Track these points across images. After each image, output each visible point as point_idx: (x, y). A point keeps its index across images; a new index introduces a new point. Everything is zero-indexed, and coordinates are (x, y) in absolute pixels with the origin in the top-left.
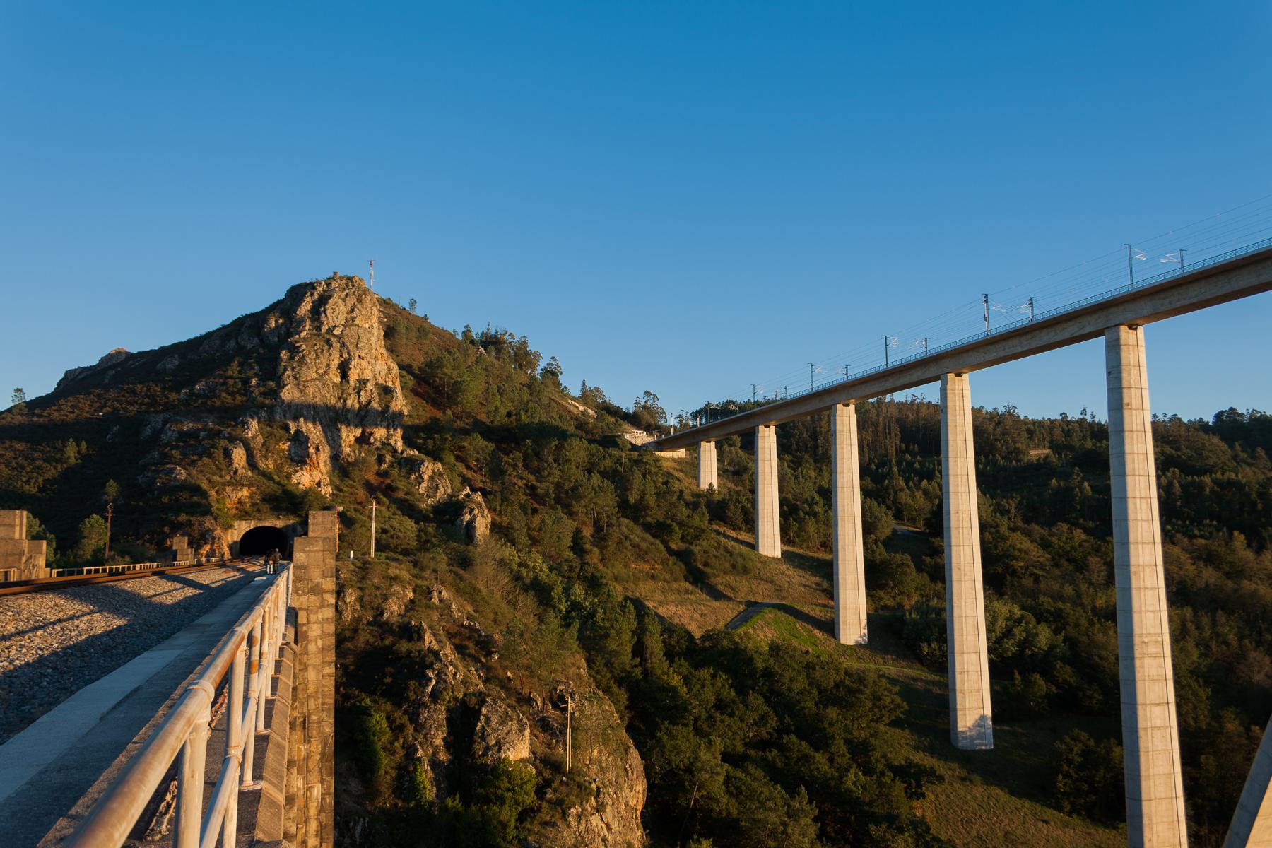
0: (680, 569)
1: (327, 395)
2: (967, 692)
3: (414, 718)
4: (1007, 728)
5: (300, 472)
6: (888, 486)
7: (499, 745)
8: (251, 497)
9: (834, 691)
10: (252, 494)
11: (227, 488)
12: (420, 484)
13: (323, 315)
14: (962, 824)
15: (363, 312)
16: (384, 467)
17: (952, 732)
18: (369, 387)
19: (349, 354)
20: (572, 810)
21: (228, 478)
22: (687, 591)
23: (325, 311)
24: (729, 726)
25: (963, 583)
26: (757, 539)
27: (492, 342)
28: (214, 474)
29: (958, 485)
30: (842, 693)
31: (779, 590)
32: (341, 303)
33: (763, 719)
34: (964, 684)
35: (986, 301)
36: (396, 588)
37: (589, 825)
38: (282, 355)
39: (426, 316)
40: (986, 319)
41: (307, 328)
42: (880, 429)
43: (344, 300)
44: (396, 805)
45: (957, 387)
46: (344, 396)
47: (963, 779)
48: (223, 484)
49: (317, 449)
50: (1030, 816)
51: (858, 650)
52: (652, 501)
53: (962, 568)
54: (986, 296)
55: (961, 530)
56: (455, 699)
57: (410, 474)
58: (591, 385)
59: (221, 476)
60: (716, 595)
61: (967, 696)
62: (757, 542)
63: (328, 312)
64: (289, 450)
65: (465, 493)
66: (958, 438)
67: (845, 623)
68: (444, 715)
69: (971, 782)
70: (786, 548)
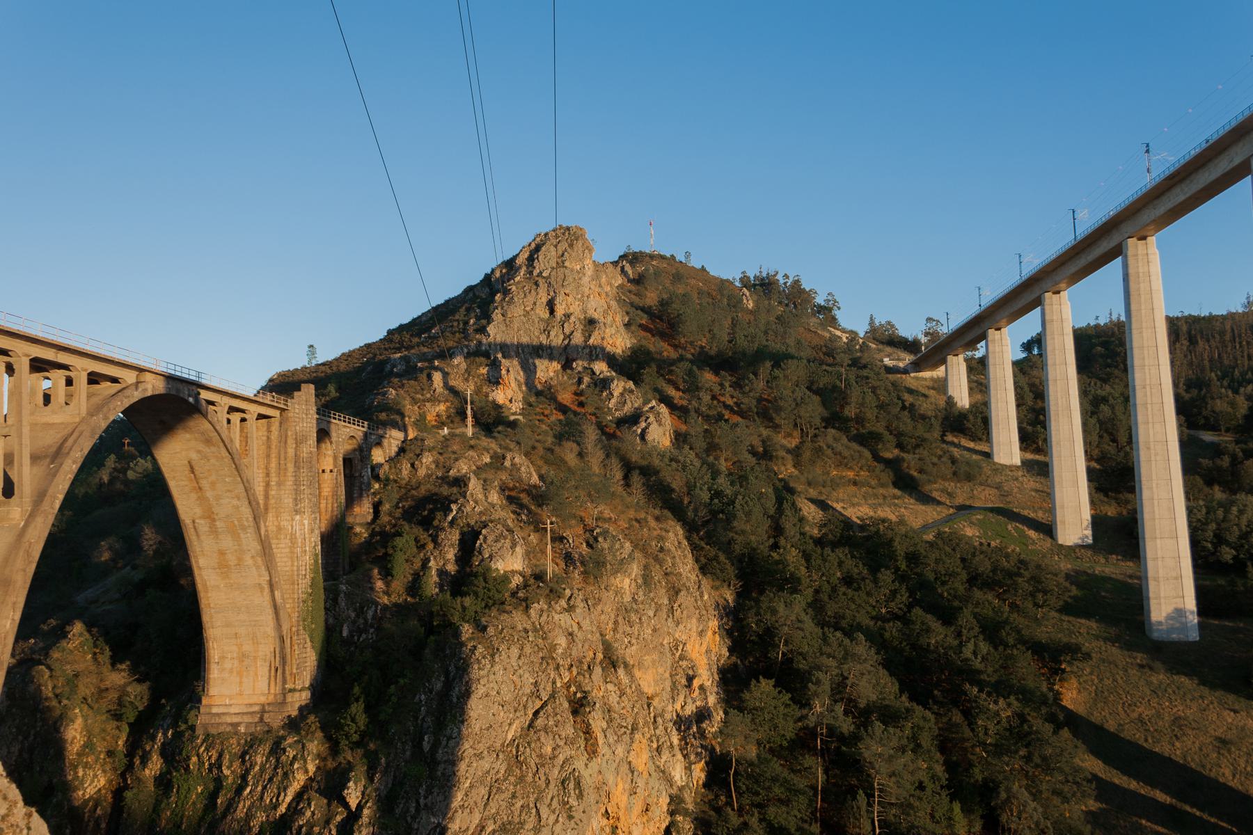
0: (887, 477)
1: (531, 328)
2: (1161, 579)
3: (435, 540)
4: (1231, 624)
5: (496, 391)
6: (1205, 396)
7: (491, 557)
8: (447, 411)
9: (991, 574)
10: (448, 408)
11: (427, 404)
12: (610, 400)
13: (536, 261)
14: (1123, 708)
15: (574, 254)
16: (583, 386)
17: (1146, 622)
18: (572, 319)
19: (554, 292)
20: (536, 605)
21: (428, 396)
22: (895, 497)
23: (537, 258)
24: (852, 600)
25: (1153, 463)
26: (991, 447)
27: (765, 285)
28: (417, 393)
29: (1144, 359)
30: (999, 576)
31: (1005, 496)
32: (552, 248)
33: (894, 593)
34: (1158, 572)
35: (1147, 151)
36: (471, 453)
37: (550, 618)
38: (496, 298)
39: (703, 266)
40: (1148, 171)
41: (522, 274)
42: (1228, 337)
43: (556, 246)
44: (406, 599)
45: (1140, 252)
46: (549, 328)
47: (1142, 666)
48: (424, 401)
49: (508, 371)
50: (1216, 704)
51: (1077, 550)
52: (870, 414)
53: (1152, 447)
54: (1148, 146)
55: (1149, 406)
56: (468, 525)
57: (602, 392)
58: (880, 320)
59: (422, 395)
60: (926, 499)
61: (1162, 584)
62: (992, 450)
63: (540, 258)
64: (488, 373)
65: (650, 405)
66: (1143, 307)
67: (1063, 522)
68: (458, 537)
69: (1151, 668)
70: (1029, 456)
